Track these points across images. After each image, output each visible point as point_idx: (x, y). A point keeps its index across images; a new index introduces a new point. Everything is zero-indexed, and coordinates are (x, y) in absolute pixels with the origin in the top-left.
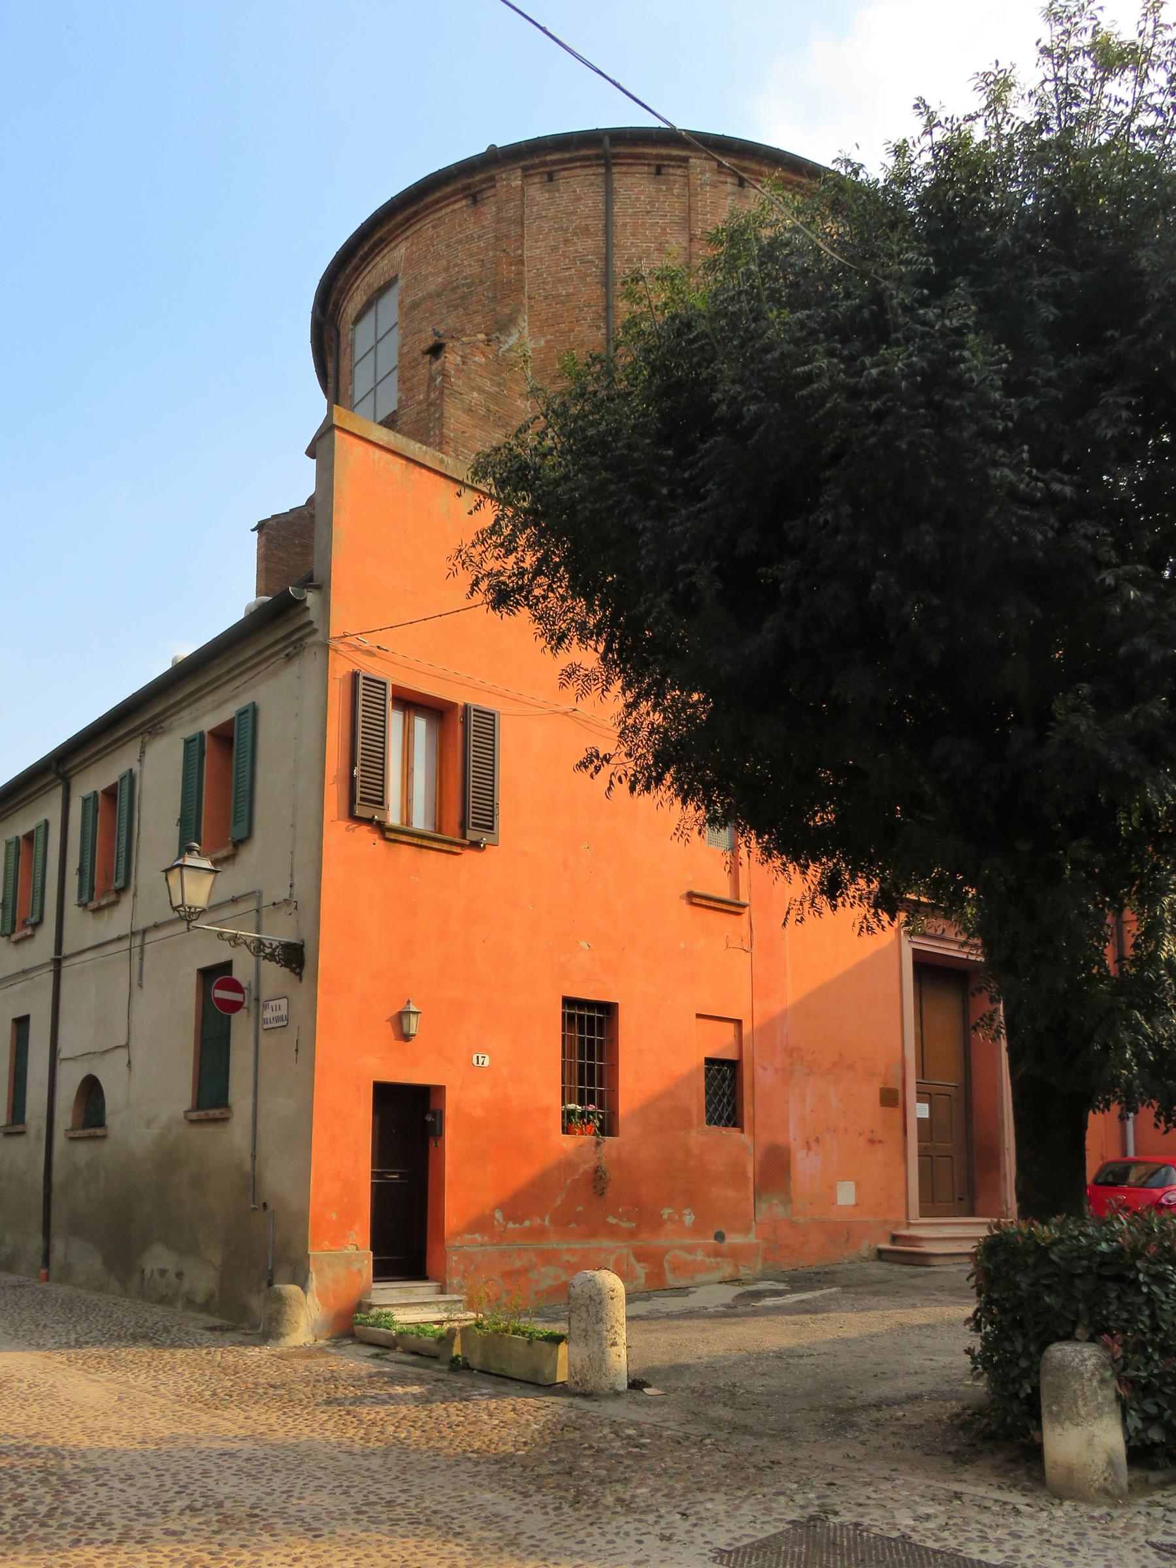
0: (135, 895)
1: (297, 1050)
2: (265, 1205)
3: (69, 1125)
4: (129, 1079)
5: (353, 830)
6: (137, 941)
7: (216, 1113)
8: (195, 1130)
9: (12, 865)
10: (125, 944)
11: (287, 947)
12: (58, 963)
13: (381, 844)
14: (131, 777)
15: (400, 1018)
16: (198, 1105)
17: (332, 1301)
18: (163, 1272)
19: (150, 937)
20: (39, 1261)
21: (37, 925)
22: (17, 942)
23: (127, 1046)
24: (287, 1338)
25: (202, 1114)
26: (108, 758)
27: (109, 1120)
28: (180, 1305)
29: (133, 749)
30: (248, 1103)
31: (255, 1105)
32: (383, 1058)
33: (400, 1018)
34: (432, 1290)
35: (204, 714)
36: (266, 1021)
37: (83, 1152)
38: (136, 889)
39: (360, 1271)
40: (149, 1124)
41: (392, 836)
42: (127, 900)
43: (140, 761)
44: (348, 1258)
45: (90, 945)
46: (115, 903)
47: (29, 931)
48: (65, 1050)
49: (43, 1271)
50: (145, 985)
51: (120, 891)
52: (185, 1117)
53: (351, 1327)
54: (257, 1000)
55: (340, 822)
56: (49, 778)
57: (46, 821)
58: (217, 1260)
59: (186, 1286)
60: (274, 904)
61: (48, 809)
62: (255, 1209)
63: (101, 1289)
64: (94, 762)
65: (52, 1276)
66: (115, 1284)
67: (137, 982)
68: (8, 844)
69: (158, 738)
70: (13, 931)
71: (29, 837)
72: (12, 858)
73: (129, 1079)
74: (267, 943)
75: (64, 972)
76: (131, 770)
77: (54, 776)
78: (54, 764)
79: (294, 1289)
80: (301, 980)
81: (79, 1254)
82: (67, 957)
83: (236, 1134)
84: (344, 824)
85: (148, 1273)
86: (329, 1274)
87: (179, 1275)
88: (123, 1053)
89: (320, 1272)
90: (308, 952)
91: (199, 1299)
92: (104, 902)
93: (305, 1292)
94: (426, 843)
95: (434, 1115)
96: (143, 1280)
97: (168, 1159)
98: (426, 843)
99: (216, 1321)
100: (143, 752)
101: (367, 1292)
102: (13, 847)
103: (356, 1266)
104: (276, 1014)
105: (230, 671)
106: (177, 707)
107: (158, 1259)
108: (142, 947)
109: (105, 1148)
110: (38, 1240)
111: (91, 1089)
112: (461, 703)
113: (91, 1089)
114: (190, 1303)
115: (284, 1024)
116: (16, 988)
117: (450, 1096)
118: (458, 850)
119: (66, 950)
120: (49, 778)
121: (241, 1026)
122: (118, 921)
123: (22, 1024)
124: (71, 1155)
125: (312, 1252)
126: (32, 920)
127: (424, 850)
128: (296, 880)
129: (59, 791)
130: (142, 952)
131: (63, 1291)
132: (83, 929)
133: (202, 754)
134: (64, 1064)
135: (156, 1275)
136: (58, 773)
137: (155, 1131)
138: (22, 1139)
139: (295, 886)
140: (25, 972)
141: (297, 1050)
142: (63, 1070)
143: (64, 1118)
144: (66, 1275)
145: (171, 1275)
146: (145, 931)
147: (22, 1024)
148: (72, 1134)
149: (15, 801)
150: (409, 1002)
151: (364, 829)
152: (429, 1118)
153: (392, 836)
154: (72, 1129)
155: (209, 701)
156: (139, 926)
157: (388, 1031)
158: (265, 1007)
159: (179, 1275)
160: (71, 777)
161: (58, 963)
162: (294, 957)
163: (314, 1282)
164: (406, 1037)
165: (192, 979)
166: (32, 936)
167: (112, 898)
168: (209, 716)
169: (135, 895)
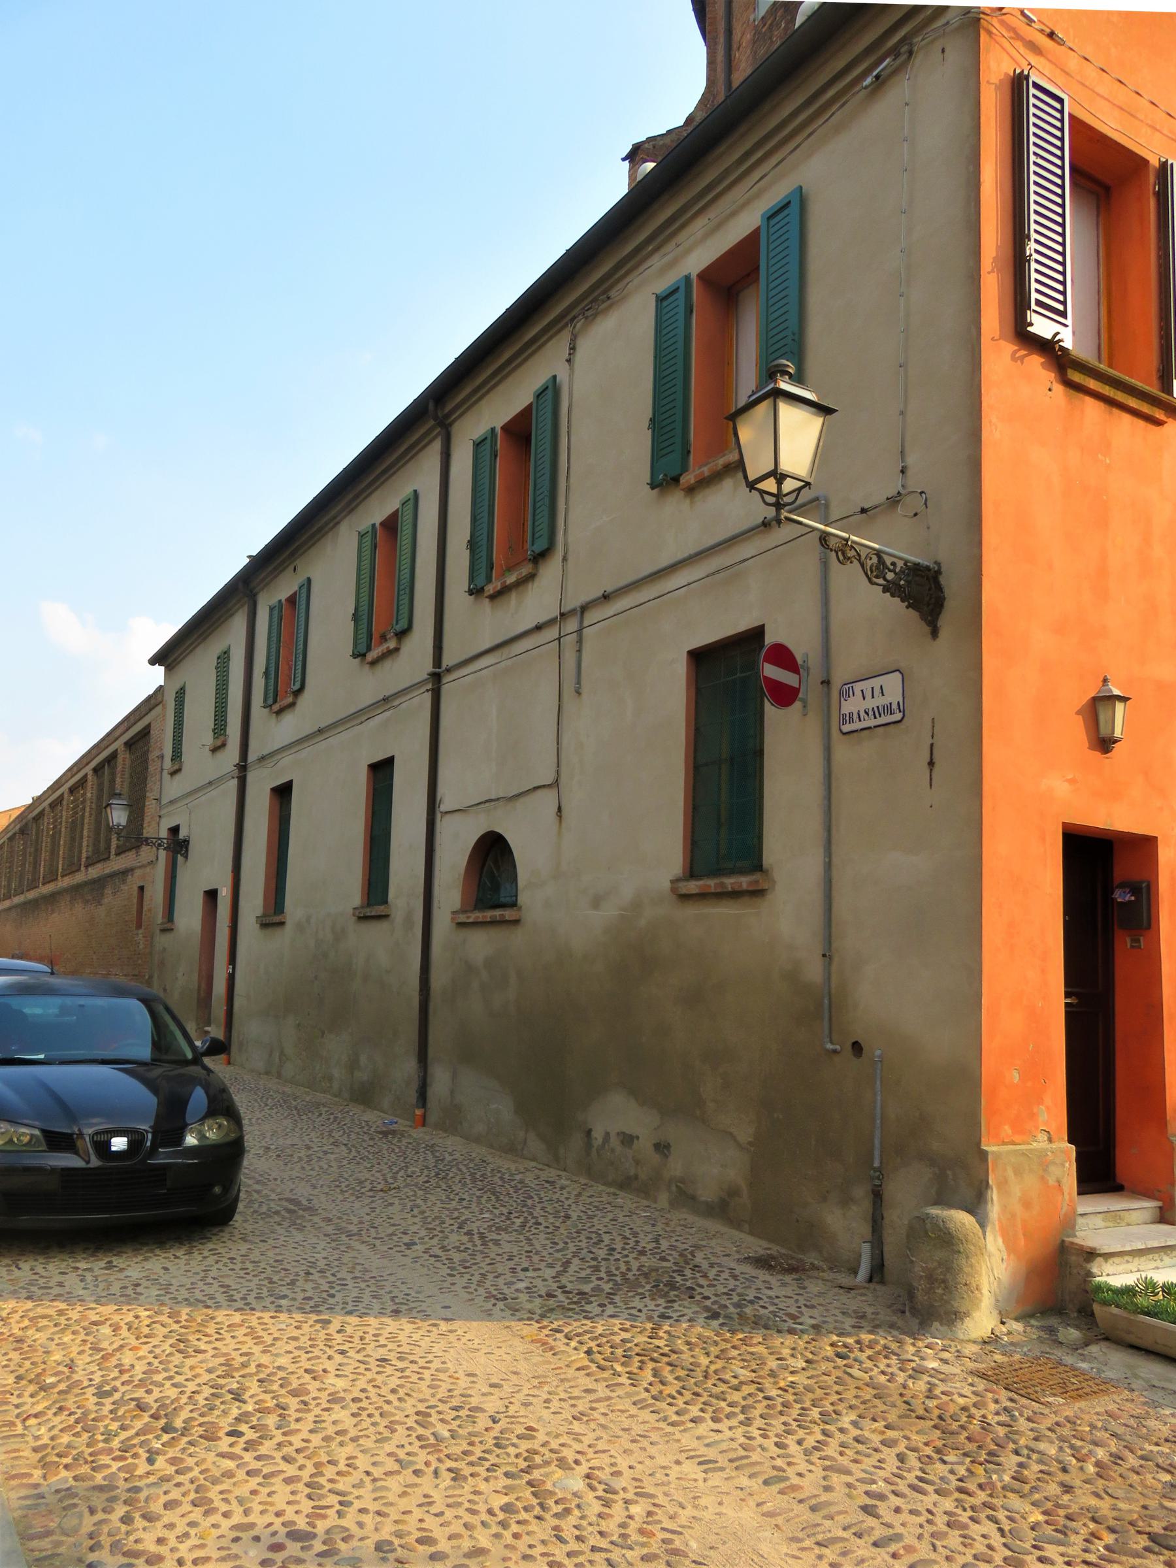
0: (565, 559)
1: (931, 764)
2: (857, 1048)
3: (457, 905)
4: (559, 833)
5: (1022, 358)
6: (572, 625)
7: (744, 882)
8: (691, 911)
9: (366, 563)
10: (551, 633)
11: (915, 570)
12: (436, 678)
13: (1059, 388)
14: (551, 392)
15: (1099, 705)
16: (692, 873)
17: (1022, 1242)
18: (628, 1140)
19: (591, 617)
20: (412, 1096)
21: (402, 634)
22: (373, 663)
23: (555, 784)
24: (967, 1320)
25: (693, 887)
26: (510, 379)
27: (522, 899)
28: (663, 1199)
29: (557, 348)
30: (810, 867)
31: (828, 866)
32: (1072, 781)
33: (1099, 705)
34: (1147, 1215)
35: (689, 251)
36: (846, 718)
37: (481, 945)
38: (566, 545)
39: (1059, 1182)
40: (597, 902)
41: (1076, 377)
42: (550, 572)
43: (569, 361)
44: (1042, 1154)
45: (487, 646)
46: (531, 577)
47: (392, 644)
48: (448, 798)
49: (419, 1112)
50: (585, 690)
51: (541, 557)
52: (673, 890)
53: (1061, 1292)
54: (826, 683)
55: (1003, 343)
56: (427, 427)
57: (415, 491)
58: (745, 1133)
59: (675, 1167)
60: (863, 511)
61: (422, 476)
62: (835, 1052)
63: (512, 1149)
64: (488, 392)
65: (433, 1118)
66: (535, 1145)
67: (572, 685)
68: (361, 536)
69: (599, 319)
70: (369, 649)
71: (391, 525)
72: (367, 553)
73: (559, 833)
74: (888, 560)
75: (445, 689)
76: (555, 377)
77: (432, 422)
78: (431, 406)
79: (961, 1219)
80: (935, 633)
81: (489, 1102)
82: (448, 670)
83: (785, 917)
84: (1009, 348)
85: (598, 1135)
86: (1016, 1190)
87: (662, 1148)
88: (550, 797)
89: (1003, 1184)
90: (952, 584)
91: (707, 1194)
92: (511, 579)
93: (983, 1226)
94: (1120, 396)
95: (1136, 889)
96: (588, 1145)
97: (635, 957)
98: (1120, 396)
99: (758, 1246)
100: (573, 349)
101: (1069, 1223)
102: (368, 538)
103: (1055, 1172)
104: (870, 704)
105: (747, 155)
106: (638, 257)
107: (618, 1116)
108: (580, 631)
109: (516, 939)
110: (408, 1067)
111: (492, 853)
112: (1154, 162)
113: (492, 853)
114: (684, 1197)
115: (892, 720)
116: (371, 723)
117: (1166, 855)
118: (1159, 415)
119: (447, 661)
120: (427, 427)
121: (787, 736)
122: (538, 601)
123: (382, 770)
124: (463, 948)
125: (990, 1147)
126: (398, 628)
127: (1115, 411)
128: (910, 460)
129: (437, 446)
130: (580, 641)
131: (452, 1146)
132: (473, 625)
133: (689, 310)
134: (448, 818)
135: (614, 1142)
136: (436, 418)
137: (610, 911)
138: (383, 925)
139: (909, 473)
140: (386, 700)
141: (931, 764)
142: (445, 827)
143: (450, 893)
144: (452, 1121)
145: (645, 1145)
146: (584, 609)
147: (382, 770)
148: (462, 918)
149: (371, 478)
150: (1105, 681)
151: (1036, 361)
152: (1122, 896)
153: (1076, 377)
154: (463, 911)
155: (699, 225)
156: (573, 603)
157: (1077, 732)
158: (845, 694)
159: (662, 1148)
160: (451, 424)
161: (436, 678)
162: (926, 593)
163: (994, 1209)
164: (1105, 744)
165: (680, 668)
166: (397, 650)
167: (525, 570)
168: (698, 250)
169: (565, 559)
